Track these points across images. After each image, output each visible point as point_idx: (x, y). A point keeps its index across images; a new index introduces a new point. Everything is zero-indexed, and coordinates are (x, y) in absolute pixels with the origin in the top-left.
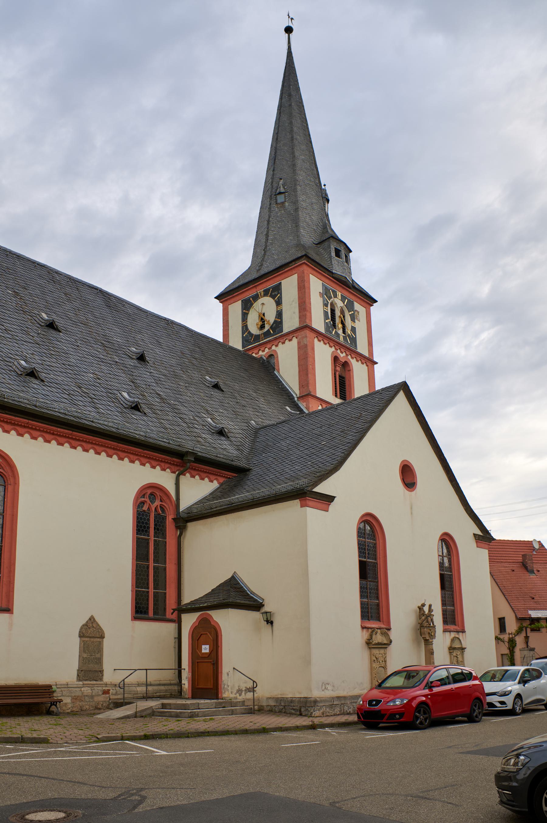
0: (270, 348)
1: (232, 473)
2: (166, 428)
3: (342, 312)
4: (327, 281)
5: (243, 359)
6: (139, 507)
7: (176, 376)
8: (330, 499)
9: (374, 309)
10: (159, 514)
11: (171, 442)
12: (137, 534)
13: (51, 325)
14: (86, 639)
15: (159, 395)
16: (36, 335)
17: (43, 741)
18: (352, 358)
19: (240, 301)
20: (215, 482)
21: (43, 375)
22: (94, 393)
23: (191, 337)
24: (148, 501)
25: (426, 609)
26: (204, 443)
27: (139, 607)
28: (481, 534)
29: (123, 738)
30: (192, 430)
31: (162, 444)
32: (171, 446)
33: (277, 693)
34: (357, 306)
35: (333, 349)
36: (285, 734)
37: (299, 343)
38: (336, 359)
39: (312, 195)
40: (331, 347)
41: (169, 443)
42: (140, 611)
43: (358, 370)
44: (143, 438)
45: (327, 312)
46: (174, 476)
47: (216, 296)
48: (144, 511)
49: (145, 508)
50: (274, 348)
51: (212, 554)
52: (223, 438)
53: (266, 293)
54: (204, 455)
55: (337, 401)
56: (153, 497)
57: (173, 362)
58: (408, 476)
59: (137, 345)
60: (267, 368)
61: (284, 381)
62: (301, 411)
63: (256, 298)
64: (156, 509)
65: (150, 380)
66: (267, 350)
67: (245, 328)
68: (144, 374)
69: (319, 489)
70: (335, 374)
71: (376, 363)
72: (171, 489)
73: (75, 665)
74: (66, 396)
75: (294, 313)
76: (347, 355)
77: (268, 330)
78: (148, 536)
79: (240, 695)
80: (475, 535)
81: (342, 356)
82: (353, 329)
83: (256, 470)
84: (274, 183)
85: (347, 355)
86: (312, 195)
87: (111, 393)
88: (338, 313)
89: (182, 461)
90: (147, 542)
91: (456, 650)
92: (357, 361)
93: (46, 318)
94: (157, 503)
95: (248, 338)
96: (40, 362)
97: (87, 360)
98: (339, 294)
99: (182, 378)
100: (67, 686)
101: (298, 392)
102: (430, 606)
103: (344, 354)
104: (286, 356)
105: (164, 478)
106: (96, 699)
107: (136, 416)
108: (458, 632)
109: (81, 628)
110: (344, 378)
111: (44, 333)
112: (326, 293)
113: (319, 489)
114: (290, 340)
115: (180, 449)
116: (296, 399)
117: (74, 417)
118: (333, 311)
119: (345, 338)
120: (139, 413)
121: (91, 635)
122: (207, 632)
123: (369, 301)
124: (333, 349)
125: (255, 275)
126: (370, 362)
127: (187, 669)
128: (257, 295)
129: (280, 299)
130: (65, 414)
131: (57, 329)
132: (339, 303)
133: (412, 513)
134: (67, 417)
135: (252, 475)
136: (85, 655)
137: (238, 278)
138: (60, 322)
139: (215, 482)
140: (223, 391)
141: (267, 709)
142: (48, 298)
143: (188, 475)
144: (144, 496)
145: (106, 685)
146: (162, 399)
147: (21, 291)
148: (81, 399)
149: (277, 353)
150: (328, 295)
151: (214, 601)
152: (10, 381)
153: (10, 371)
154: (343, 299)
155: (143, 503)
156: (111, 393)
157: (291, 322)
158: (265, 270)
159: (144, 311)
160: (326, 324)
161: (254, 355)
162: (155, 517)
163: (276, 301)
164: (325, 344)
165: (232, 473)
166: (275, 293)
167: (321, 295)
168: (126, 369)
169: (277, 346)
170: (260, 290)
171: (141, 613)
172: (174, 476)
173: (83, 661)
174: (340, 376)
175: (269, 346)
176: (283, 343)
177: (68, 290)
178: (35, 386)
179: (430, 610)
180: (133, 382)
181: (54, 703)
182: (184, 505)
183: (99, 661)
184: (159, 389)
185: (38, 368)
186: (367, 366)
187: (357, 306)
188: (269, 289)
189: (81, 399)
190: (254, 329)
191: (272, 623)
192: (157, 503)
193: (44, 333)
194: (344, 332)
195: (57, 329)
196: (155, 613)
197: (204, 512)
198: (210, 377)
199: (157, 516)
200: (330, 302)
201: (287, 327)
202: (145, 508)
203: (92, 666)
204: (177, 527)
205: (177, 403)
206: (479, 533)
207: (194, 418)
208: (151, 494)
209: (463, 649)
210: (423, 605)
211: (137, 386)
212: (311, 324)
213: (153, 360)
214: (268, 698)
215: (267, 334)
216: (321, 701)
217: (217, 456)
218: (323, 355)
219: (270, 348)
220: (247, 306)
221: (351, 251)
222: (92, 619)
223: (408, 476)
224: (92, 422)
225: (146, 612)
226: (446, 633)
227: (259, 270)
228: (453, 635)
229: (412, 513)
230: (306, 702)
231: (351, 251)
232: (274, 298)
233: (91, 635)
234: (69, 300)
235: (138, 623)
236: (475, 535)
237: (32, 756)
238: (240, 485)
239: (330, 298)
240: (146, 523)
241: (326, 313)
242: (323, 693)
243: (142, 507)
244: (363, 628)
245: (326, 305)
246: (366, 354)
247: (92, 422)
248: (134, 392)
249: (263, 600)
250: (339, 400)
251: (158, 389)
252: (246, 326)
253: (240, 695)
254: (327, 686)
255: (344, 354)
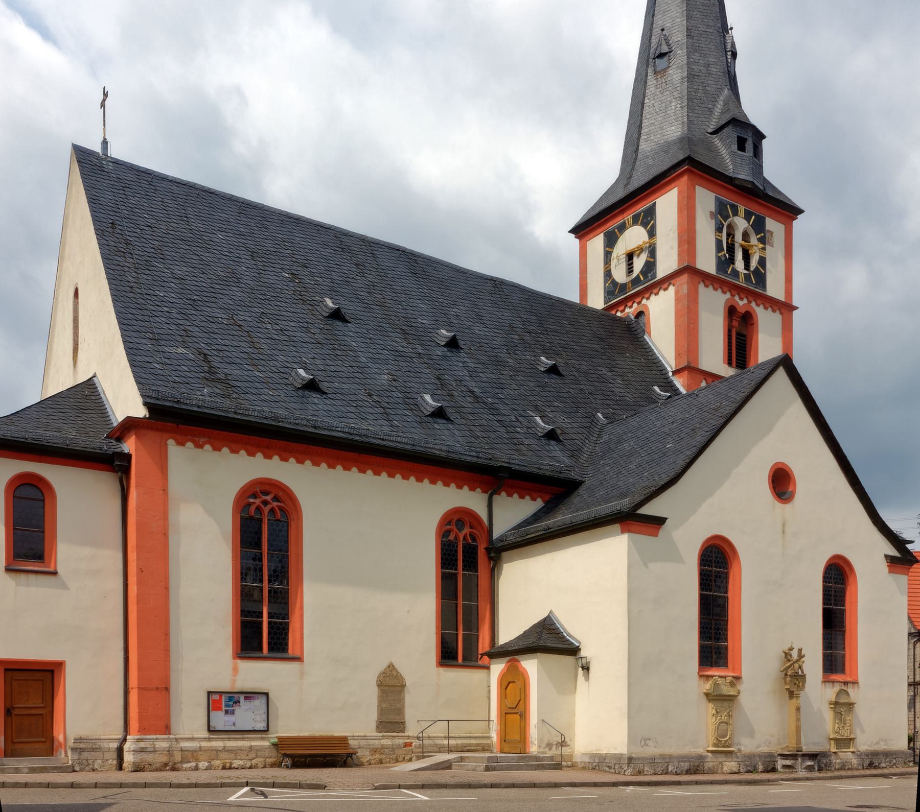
0: (639, 303)
1: (556, 490)
3: (746, 236)
5: (605, 317)
6: (443, 536)
7: (499, 363)
8: (660, 521)
9: (798, 224)
10: (469, 544)
12: (442, 568)
13: (337, 315)
14: (385, 688)
15: (472, 392)
16: (318, 331)
18: (758, 305)
19: (602, 235)
20: (539, 500)
21: (324, 386)
22: (387, 400)
25: (795, 654)
27: (447, 652)
28: (898, 555)
30: (511, 435)
31: (469, 459)
32: (480, 461)
34: (771, 224)
35: (728, 295)
37: (676, 292)
38: (731, 311)
40: (724, 293)
41: (478, 457)
46: (486, 496)
49: (452, 537)
50: (644, 301)
51: (527, 590)
52: (553, 442)
55: (727, 372)
56: (460, 523)
57: (498, 341)
58: (781, 482)
59: (449, 326)
60: (633, 333)
61: (657, 348)
62: (676, 391)
63: (622, 228)
64: (465, 538)
65: (463, 373)
66: (635, 305)
67: (608, 274)
68: (459, 365)
70: (730, 331)
71: (796, 308)
72: (483, 514)
73: (373, 716)
74: (352, 409)
75: (672, 248)
76: (749, 302)
77: (638, 276)
79: (550, 749)
80: (886, 556)
81: (742, 303)
82: (762, 262)
85: (749, 302)
87: (409, 398)
88: (739, 238)
89: (494, 478)
90: (455, 576)
91: (842, 707)
92: (766, 308)
94: (466, 530)
95: (612, 288)
97: (381, 357)
98: (742, 209)
100: (365, 738)
102: (800, 650)
103: (745, 301)
105: (472, 500)
108: (846, 683)
109: (379, 676)
110: (744, 336)
112: (722, 212)
114: (666, 289)
115: (492, 463)
116: (670, 374)
118: (730, 235)
119: (747, 277)
120: (445, 421)
121: (391, 686)
123: (789, 211)
124: (728, 295)
125: (620, 194)
127: (495, 722)
128: (624, 223)
130: (350, 434)
131: (344, 320)
132: (741, 224)
133: (783, 532)
134: (351, 437)
135: (581, 490)
136: (384, 705)
137: (596, 204)
138: (348, 309)
139: (539, 500)
141: (581, 766)
143: (503, 494)
144: (449, 523)
145: (409, 737)
150: (724, 213)
151: (522, 645)
152: (286, 399)
153: (286, 385)
154: (748, 216)
155: (448, 532)
156: (409, 398)
157: (667, 263)
158: (636, 183)
159: (462, 272)
160: (719, 259)
161: (619, 314)
162: (464, 547)
163: (648, 232)
164: (715, 289)
165: (556, 490)
166: (648, 219)
168: (432, 362)
169: (648, 298)
170: (628, 217)
171: (449, 658)
172: (486, 496)
173: (381, 712)
174: (737, 334)
175: (637, 300)
178: (316, 401)
179: (801, 656)
180: (439, 379)
181: (350, 755)
182: (497, 533)
183: (400, 711)
185: (320, 376)
186: (781, 313)
187: (771, 224)
188: (639, 214)
191: (588, 669)
192: (466, 530)
194: (747, 266)
195: (344, 320)
196: (464, 660)
197: (529, 539)
198: (547, 358)
200: (726, 224)
201: (664, 268)
202: (452, 537)
203: (392, 717)
204: (490, 559)
205: (496, 401)
208: (459, 520)
210: (791, 649)
215: (636, 282)
216: (638, 759)
217: (540, 469)
218: (713, 308)
219: (639, 303)
220: (611, 241)
222: (391, 667)
223: (781, 482)
224: (383, 440)
225: (455, 658)
226: (827, 684)
228: (837, 688)
229: (783, 532)
230: (620, 759)
232: (645, 227)
233: (391, 686)
234: (362, 274)
236: (886, 556)
238: (562, 506)
239: (726, 218)
240: (453, 555)
241: (719, 243)
243: (448, 536)
244: (701, 676)
245: (719, 229)
246: (781, 297)
247: (383, 440)
248: (439, 392)
249: (580, 643)
250: (733, 370)
251: (472, 385)
253: (550, 749)
254: (648, 742)
255: (745, 301)
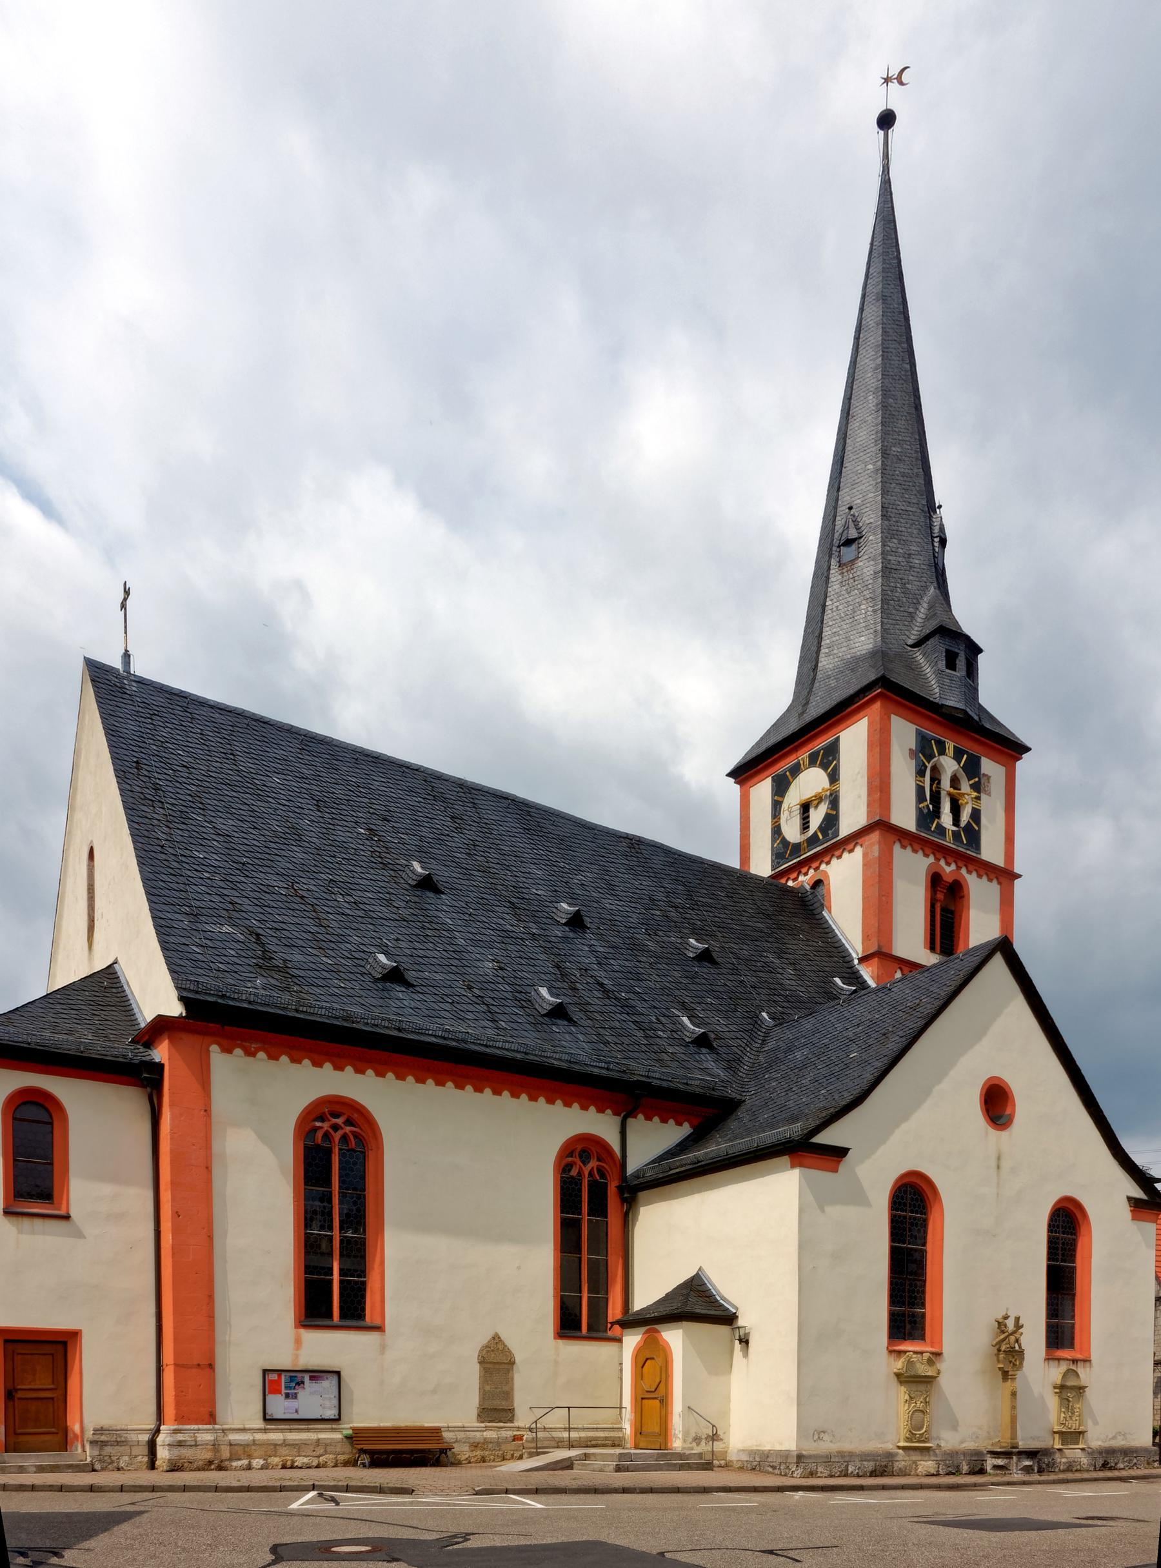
0: (817, 869)
1: (707, 1112)
2: (607, 1043)
3: (955, 782)
4: (927, 724)
5: (773, 887)
6: (564, 1171)
8: (841, 1153)
9: (1023, 766)
11: (611, 1066)
13: (427, 884)
14: (488, 1366)
15: (601, 985)
16: (403, 904)
17: (410, 1492)
18: (969, 872)
19: (770, 779)
20: (686, 1125)
21: (411, 976)
22: (492, 995)
23: (672, 865)
24: (579, 1163)
26: (669, 1063)
29: (507, 1492)
31: (596, 1071)
32: (611, 1074)
33: (751, 1444)
34: (988, 766)
35: (931, 859)
36: (731, 1495)
37: (865, 855)
39: (911, 535)
42: (569, 1324)
43: (981, 895)
44: (564, 1065)
45: (923, 788)
46: (618, 1119)
47: (728, 771)
48: (572, 1177)
49: (574, 1172)
50: (823, 867)
51: (672, 1240)
52: (704, 1050)
53: (813, 761)
54: (665, 1084)
55: (928, 958)
56: (585, 1156)
57: (634, 918)
58: (996, 1102)
59: (572, 898)
60: (808, 908)
62: (863, 985)
63: (796, 770)
66: (812, 871)
67: (777, 831)
69: (823, 1138)
71: (1019, 876)
76: (959, 868)
78: (580, 1214)
80: (1129, 1199)
81: (948, 869)
82: (976, 815)
83: (751, 1101)
84: (838, 518)
85: (959, 868)
86: (911, 535)
88: (946, 784)
92: (980, 876)
93: (419, 870)
95: (782, 849)
96: (408, 952)
98: (950, 746)
99: (646, 948)
100: (463, 1429)
101: (859, 948)
102: (1017, 1319)
103: (953, 867)
104: (844, 882)
105: (602, 1125)
106: (503, 1447)
107: (559, 1028)
109: (481, 1351)
110: (952, 912)
111: (417, 899)
112: (925, 750)
113: (823, 1138)
114: (851, 851)
116: (856, 962)
117: (457, 1041)
121: (496, 1363)
122: (652, 1359)
123: (1011, 749)
124: (931, 859)
125: (793, 726)
126: (1005, 876)
127: (629, 1408)
129: (836, 771)
130: (445, 1038)
132: (949, 765)
133: (998, 1167)
135: (741, 1113)
136: (488, 1388)
140: (717, 963)
142: (424, 832)
143: (641, 1117)
144: (571, 1154)
146: (606, 991)
147: (382, 827)
148: (470, 1008)
149: (828, 877)
150: (927, 752)
151: (663, 1311)
152: (362, 993)
153: (362, 974)
157: (853, 817)
158: (814, 711)
160: (920, 811)
161: (790, 883)
165: (707, 1112)
166: (828, 759)
167: (913, 754)
169: (828, 863)
170: (803, 756)
172: (618, 1119)
173: (484, 1395)
175: (815, 865)
176: (839, 857)
177: (459, 808)
182: (631, 1168)
183: (508, 1395)
184: (603, 974)
185: (406, 962)
186: (1000, 883)
187: (988, 766)
188: (818, 752)
189: (470, 1008)
190: (792, 832)
191: (747, 1342)
192: (593, 1163)
193: (417, 899)
194: (956, 821)
196: (590, 1329)
198: (696, 940)
199: (593, 1185)
200: (929, 766)
201: (848, 825)
202: (574, 1172)
204: (623, 1200)
205: (632, 996)
206: (1139, 1193)
207: (658, 1019)
208: (583, 1151)
209: (1080, 1389)
210: (1006, 1317)
211: (564, 975)
212: (889, 817)
213: (596, 920)
214: (739, 1451)
215: (813, 841)
216: (810, 1457)
218: (911, 874)
220: (781, 787)
221: (980, 651)
222: (496, 1338)
223: (996, 1102)
224: (486, 1046)
227: (803, 712)
229: (998, 1167)
231: (980, 651)
233: (496, 1363)
235: (560, 1342)
236: (1129, 1199)
237: (382, 1504)
238: (715, 1135)
239: (930, 757)
241: (920, 790)
242: (815, 1444)
243: (569, 1171)
244: (891, 1352)
245: (921, 773)
248: (559, 985)
249: (737, 1309)
250: (937, 956)
251: (601, 975)
252: (779, 827)
254: (822, 1435)
255: (953, 867)
